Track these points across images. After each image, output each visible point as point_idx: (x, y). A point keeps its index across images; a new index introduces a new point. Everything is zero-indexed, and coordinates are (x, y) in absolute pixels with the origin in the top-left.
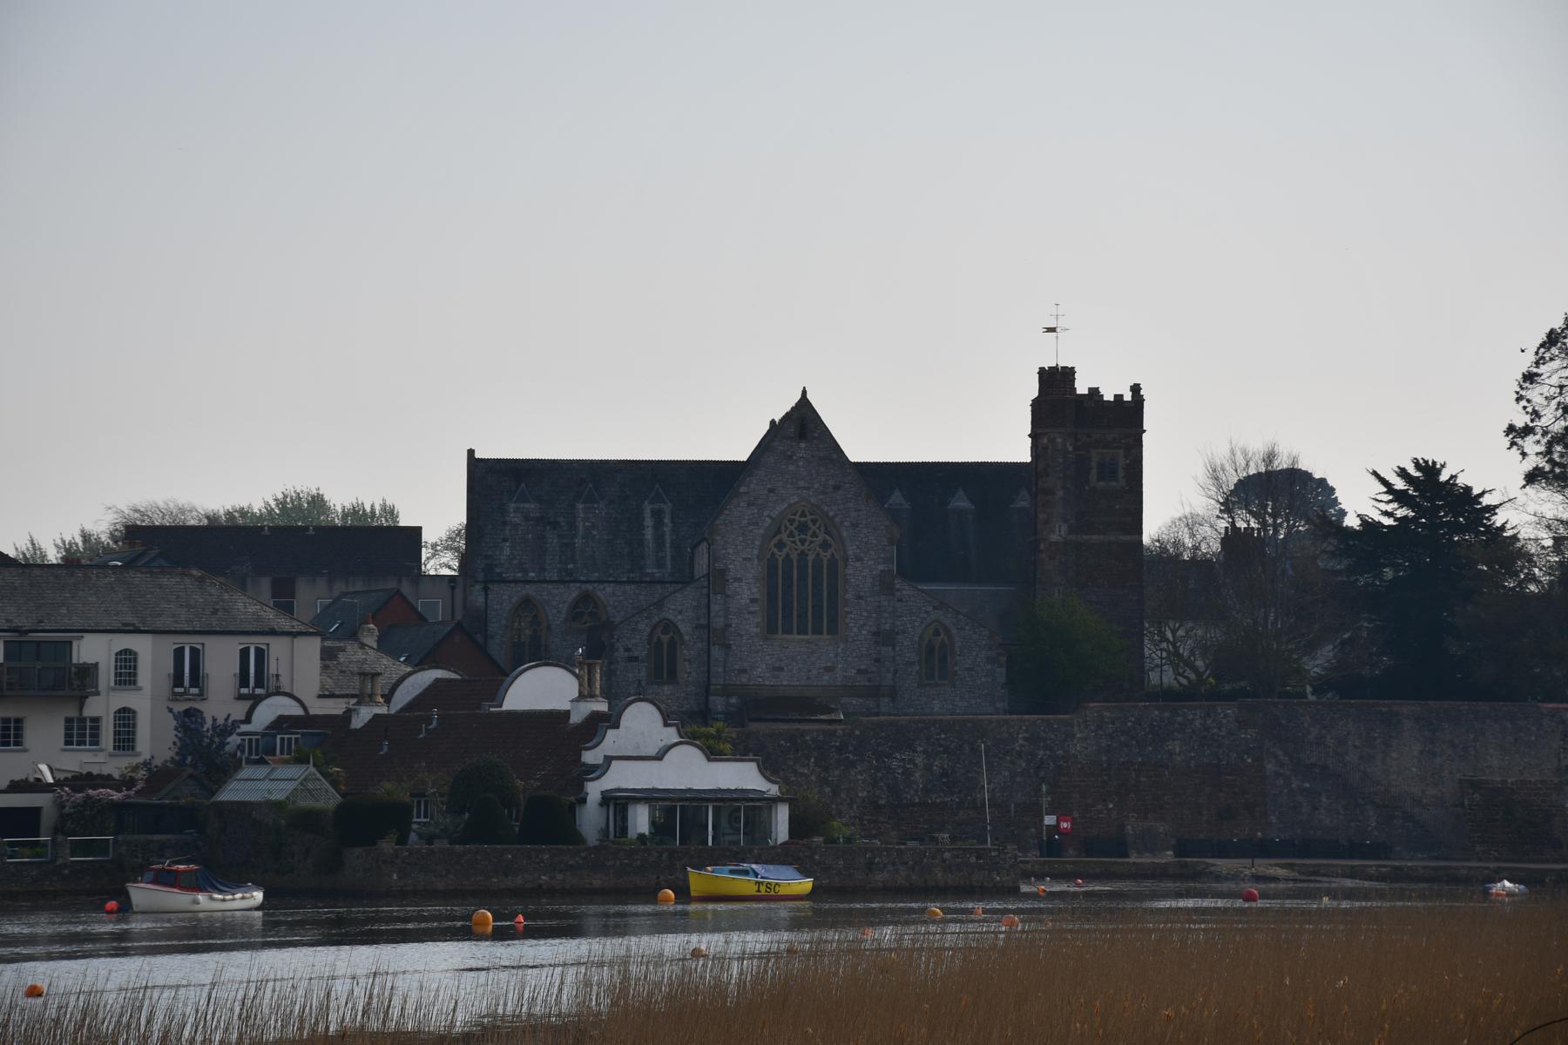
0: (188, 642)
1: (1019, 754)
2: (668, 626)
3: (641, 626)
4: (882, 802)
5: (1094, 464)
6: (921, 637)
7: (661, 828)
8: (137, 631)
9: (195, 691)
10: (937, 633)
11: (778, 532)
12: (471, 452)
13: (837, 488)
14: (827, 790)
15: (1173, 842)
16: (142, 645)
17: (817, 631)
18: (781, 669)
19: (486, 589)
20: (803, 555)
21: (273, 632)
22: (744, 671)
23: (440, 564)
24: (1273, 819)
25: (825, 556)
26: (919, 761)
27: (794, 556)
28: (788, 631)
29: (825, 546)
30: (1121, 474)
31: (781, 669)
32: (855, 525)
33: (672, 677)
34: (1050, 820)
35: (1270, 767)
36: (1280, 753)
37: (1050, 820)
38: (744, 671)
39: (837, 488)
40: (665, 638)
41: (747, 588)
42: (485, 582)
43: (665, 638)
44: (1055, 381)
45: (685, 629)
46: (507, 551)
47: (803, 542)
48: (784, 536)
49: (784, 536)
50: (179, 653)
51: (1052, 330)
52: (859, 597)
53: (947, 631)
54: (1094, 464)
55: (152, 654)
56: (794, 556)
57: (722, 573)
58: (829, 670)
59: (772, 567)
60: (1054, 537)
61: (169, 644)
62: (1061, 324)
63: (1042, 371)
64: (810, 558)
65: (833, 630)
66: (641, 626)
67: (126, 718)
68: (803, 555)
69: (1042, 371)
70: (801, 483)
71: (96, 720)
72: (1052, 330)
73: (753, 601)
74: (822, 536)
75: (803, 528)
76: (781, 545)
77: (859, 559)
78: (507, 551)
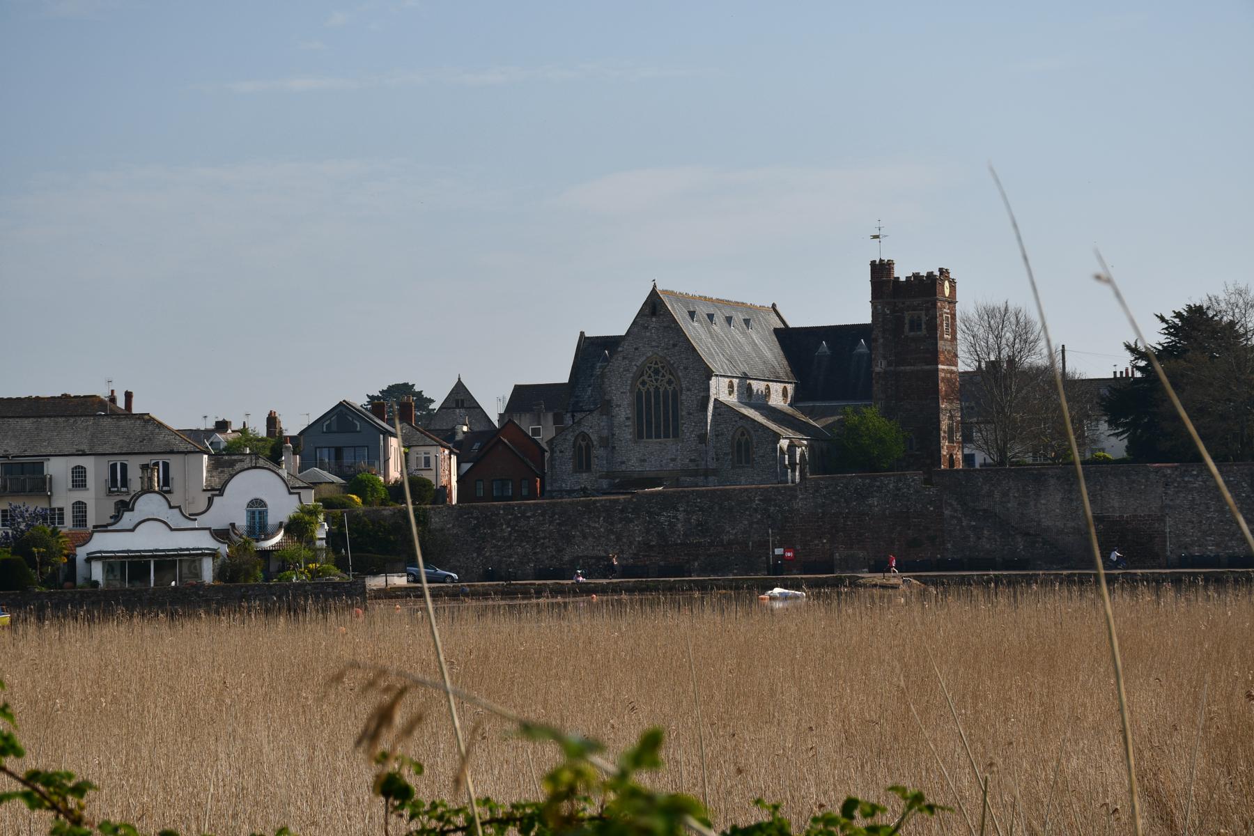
0: (119, 460)
1: (756, 510)
2: (585, 436)
3: (569, 437)
6: (733, 438)
7: (220, 574)
8: (84, 454)
9: (124, 489)
10: (743, 434)
11: (642, 375)
12: (582, 333)
13: (675, 345)
14: (612, 537)
15: (872, 563)
16: (88, 463)
17: (666, 436)
18: (644, 461)
19: (573, 416)
21: (172, 452)
22: (623, 463)
23: (435, 406)
24: (949, 546)
25: (670, 389)
26: (681, 516)
27: (652, 390)
28: (649, 437)
29: (670, 382)
30: (924, 326)
31: (644, 461)
32: (686, 368)
33: (588, 468)
34: (779, 551)
35: (947, 512)
36: (955, 503)
37: (779, 551)
38: (623, 463)
39: (675, 345)
40: (583, 444)
41: (624, 411)
42: (573, 412)
43: (583, 444)
44: (881, 271)
45: (594, 437)
46: (589, 392)
47: (657, 380)
48: (645, 378)
49: (645, 378)
50: (114, 467)
51: (877, 237)
52: (689, 414)
53: (749, 432)
54: (907, 321)
55: (95, 469)
56: (652, 390)
57: (609, 402)
58: (673, 460)
59: (639, 397)
60: (878, 369)
61: (105, 463)
62: (882, 233)
63: (873, 263)
64: (661, 390)
65: (676, 435)
66: (569, 437)
67: (80, 508)
69: (873, 263)
71: (61, 509)
72: (877, 237)
73: (628, 418)
74: (668, 376)
75: (656, 372)
76: (643, 383)
77: (689, 390)
78: (589, 392)
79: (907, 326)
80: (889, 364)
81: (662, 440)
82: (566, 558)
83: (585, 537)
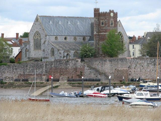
4: (22, 74)
5: (101, 22)
13: (40, 29)
20: (38, 38)
27: (37, 39)
39: (40, 29)
54: (101, 22)
68: (38, 38)
70: (37, 28)
73: (33, 45)
79: (101, 24)
80: (97, 33)
81: (38, 50)
82: (4, 77)
83: (8, 72)
